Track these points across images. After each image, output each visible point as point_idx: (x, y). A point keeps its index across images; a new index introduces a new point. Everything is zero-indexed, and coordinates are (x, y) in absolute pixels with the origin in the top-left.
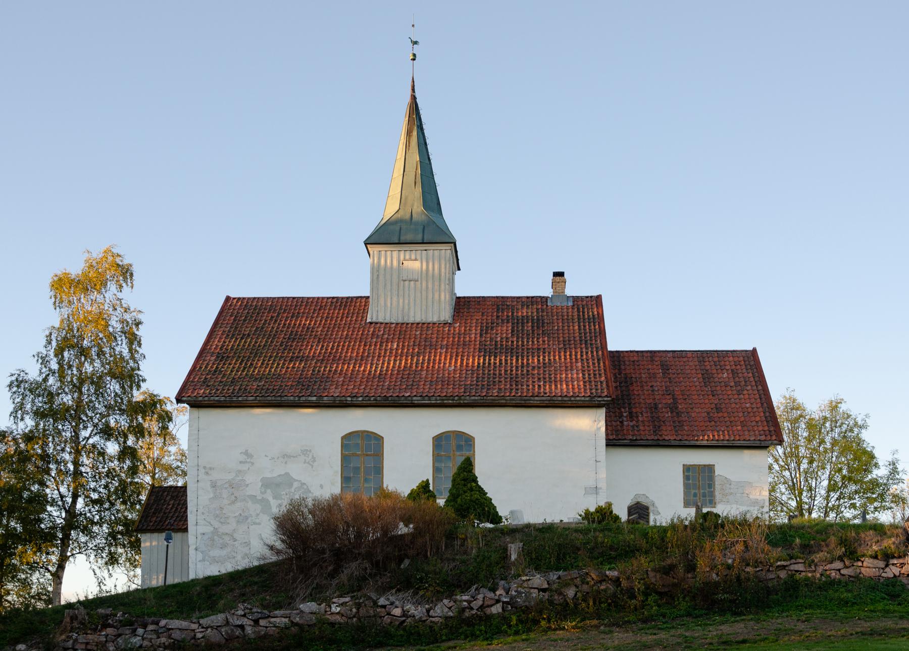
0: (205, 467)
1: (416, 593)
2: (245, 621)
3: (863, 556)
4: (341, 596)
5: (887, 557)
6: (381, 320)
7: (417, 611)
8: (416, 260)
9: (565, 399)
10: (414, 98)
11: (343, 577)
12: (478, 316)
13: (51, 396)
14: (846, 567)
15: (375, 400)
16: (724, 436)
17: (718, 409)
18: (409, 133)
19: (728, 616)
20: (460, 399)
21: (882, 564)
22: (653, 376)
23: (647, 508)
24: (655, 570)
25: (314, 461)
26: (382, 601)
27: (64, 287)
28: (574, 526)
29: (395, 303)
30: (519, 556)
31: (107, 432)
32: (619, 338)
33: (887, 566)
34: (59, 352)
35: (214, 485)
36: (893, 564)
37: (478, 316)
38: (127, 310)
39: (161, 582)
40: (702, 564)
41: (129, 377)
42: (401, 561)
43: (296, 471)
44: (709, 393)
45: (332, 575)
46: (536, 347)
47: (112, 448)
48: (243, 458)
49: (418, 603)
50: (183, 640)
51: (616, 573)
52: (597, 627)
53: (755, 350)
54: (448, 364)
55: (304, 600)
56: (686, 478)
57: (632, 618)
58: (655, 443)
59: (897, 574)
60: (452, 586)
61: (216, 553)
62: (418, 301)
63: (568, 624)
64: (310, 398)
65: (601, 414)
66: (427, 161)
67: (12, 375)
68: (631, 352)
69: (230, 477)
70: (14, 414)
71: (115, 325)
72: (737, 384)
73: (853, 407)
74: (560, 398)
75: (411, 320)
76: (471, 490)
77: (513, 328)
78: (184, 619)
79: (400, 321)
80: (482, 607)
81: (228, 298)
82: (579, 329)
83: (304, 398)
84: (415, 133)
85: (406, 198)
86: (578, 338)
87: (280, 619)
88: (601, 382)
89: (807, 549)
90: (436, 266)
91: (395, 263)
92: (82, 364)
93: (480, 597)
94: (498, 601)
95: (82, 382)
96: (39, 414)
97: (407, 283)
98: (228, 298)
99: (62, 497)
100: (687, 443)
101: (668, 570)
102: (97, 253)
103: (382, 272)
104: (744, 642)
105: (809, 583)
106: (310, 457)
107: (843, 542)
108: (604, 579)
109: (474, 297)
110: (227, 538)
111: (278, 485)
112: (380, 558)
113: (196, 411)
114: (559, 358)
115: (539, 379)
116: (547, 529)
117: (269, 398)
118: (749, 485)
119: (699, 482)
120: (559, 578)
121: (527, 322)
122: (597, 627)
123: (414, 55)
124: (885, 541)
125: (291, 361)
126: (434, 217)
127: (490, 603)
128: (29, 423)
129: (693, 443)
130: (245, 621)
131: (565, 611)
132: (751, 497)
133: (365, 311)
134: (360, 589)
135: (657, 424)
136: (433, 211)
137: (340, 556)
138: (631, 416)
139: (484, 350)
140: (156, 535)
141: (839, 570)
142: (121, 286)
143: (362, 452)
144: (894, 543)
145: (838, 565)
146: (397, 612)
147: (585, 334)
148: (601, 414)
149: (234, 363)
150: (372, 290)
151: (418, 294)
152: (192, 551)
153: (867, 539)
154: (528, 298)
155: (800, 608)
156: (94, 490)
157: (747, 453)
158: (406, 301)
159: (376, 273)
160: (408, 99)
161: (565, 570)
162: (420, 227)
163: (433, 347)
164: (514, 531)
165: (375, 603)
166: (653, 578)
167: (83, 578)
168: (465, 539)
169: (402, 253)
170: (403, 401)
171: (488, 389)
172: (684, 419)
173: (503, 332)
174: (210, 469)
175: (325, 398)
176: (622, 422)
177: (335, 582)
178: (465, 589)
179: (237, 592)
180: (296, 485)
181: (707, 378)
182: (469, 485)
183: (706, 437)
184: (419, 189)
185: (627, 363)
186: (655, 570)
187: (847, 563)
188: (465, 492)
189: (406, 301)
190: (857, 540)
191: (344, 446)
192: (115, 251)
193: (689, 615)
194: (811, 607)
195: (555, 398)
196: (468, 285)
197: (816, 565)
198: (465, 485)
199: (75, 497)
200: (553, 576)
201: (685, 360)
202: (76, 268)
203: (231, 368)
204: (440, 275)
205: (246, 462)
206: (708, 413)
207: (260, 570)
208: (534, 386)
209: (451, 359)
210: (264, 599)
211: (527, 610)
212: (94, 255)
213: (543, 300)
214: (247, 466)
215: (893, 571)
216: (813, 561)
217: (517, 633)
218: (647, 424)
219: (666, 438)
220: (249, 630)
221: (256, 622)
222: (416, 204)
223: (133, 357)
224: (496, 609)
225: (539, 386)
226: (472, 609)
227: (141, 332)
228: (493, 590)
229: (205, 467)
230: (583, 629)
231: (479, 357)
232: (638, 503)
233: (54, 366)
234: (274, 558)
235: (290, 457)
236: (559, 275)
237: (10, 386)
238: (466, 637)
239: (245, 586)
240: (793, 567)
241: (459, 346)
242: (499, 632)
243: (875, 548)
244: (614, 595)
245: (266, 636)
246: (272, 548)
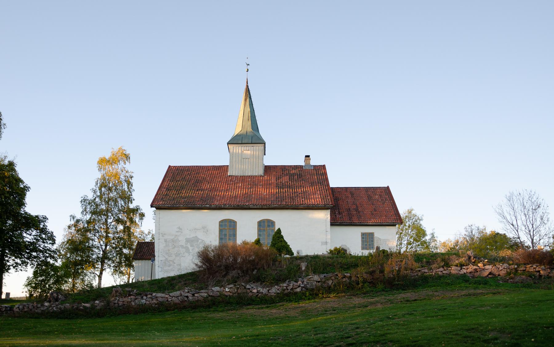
1: (261, 284)
2: (189, 294)
4: (229, 285)
5: (461, 265)
7: (265, 291)
11: (229, 277)
12: (274, 173)
13: (97, 205)
14: (445, 270)
16: (378, 221)
17: (375, 210)
18: (246, 100)
19: (400, 291)
21: (459, 268)
24: (366, 273)
26: (248, 287)
27: (103, 162)
31: (118, 221)
32: (334, 183)
34: (100, 189)
35: (166, 241)
37: (274, 173)
38: (127, 172)
39: (149, 279)
40: (387, 269)
41: (128, 198)
42: (253, 270)
43: (200, 235)
45: (224, 276)
46: (300, 185)
47: (121, 227)
48: (178, 230)
49: (263, 288)
50: (163, 302)
51: (349, 275)
52: (344, 296)
53: (388, 187)
54: (264, 192)
55: (212, 286)
56: (363, 238)
57: (359, 292)
60: (278, 280)
61: (166, 268)
63: (332, 295)
65: (329, 210)
69: (173, 237)
70: (82, 212)
71: (122, 177)
72: (382, 200)
73: (417, 212)
75: (247, 175)
76: (281, 241)
78: (163, 293)
80: (292, 289)
81: (170, 166)
84: (248, 100)
87: (204, 294)
89: (428, 263)
91: (240, 151)
92: (109, 194)
93: (291, 285)
94: (299, 286)
95: (109, 200)
96: (93, 213)
98: (170, 166)
99: (101, 245)
101: (372, 273)
102: (116, 149)
104: (415, 300)
105: (431, 277)
107: (443, 260)
108: (345, 277)
110: (171, 262)
112: (245, 269)
113: (158, 211)
114: (309, 189)
116: (316, 257)
118: (388, 239)
119: (367, 240)
120: (325, 276)
122: (344, 296)
126: (256, 133)
127: (296, 287)
128: (88, 217)
129: (366, 224)
130: (189, 294)
131: (329, 290)
133: (227, 171)
134: (236, 282)
135: (350, 216)
137: (228, 268)
138: (339, 213)
139: (278, 186)
140: (140, 261)
142: (125, 162)
143: (227, 228)
145: (441, 269)
146: (255, 291)
148: (329, 210)
149: (174, 192)
150: (230, 162)
152: (157, 267)
155: (430, 286)
156: (114, 243)
157: (387, 227)
160: (245, 87)
161: (327, 273)
162: (250, 137)
163: (257, 185)
164: (301, 258)
165: (245, 288)
166: (365, 276)
167: (109, 279)
168: (280, 262)
170: (245, 207)
173: (285, 179)
177: (225, 279)
178: (284, 281)
179: (183, 283)
180: (200, 241)
181: (369, 198)
184: (250, 122)
186: (366, 273)
187: (445, 268)
190: (449, 259)
191: (220, 225)
192: (123, 148)
193: (383, 291)
194: (434, 286)
196: (269, 161)
199: (106, 246)
200: (322, 276)
203: (172, 193)
207: (192, 274)
210: (195, 286)
211: (313, 290)
213: (301, 167)
214: (180, 233)
215: (464, 271)
217: (309, 299)
220: (190, 298)
221: (193, 295)
223: (129, 191)
224: (298, 290)
226: (288, 289)
227: (133, 181)
228: (296, 282)
230: (339, 297)
233: (99, 194)
234: (198, 269)
237: (81, 202)
238: (287, 301)
239: (186, 281)
240: (423, 271)
241: (267, 185)
242: (301, 299)
243: (457, 262)
244: (350, 283)
245: (198, 301)
246: (196, 265)
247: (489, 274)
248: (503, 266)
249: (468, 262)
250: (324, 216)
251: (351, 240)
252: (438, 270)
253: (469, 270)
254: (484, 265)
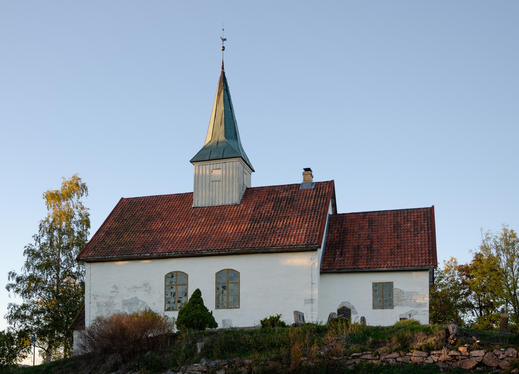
0: (94, 295)
3: (412, 349)
5: (429, 349)
6: (199, 206)
8: (219, 169)
9: (291, 247)
10: (223, 73)
15: (181, 253)
18: (219, 94)
20: (229, 251)
21: (425, 354)
22: (361, 228)
23: (350, 310)
25: (150, 290)
27: (53, 197)
28: (246, 330)
29: (207, 195)
30: (202, 350)
32: (344, 206)
33: (429, 355)
35: (98, 305)
36: (433, 354)
43: (141, 296)
44: (396, 236)
56: (374, 291)
58: (353, 270)
59: (436, 361)
62: (221, 194)
64: (146, 255)
66: (229, 110)
67: (26, 247)
68: (352, 213)
74: (288, 247)
75: (217, 204)
77: (274, 204)
79: (211, 205)
82: (314, 203)
83: (143, 255)
85: (216, 133)
86: (311, 209)
88: (316, 235)
89: (375, 345)
90: (231, 172)
91: (208, 172)
97: (214, 183)
100: (373, 269)
103: (200, 178)
106: (148, 287)
109: (257, 188)
111: (131, 304)
115: (279, 235)
117: (125, 256)
121: (284, 201)
123: (224, 47)
124: (429, 339)
125: (143, 233)
126: (232, 143)
132: (417, 301)
136: (232, 139)
138: (341, 254)
141: (396, 358)
144: (435, 340)
145: (395, 355)
147: (316, 205)
151: (221, 189)
153: (418, 337)
154: (288, 185)
157: (414, 274)
158: (214, 194)
159: (197, 178)
160: (219, 74)
162: (225, 147)
169: (201, 166)
171: (247, 244)
172: (375, 254)
174: (97, 296)
175: (154, 254)
176: (334, 258)
180: (140, 303)
182: (196, 306)
183: (386, 266)
184: (223, 127)
185: (348, 221)
188: (193, 310)
189: (214, 194)
195: (285, 247)
196: (258, 180)
197: (379, 356)
198: (193, 306)
201: (385, 216)
202: (57, 187)
204: (233, 177)
205: (115, 291)
206: (391, 250)
208: (274, 240)
209: (232, 226)
212: (67, 180)
213: (298, 186)
214: (115, 293)
216: (378, 352)
218: (350, 258)
219: (360, 267)
222: (221, 136)
225: (278, 240)
229: (94, 295)
231: (249, 224)
232: (344, 307)
235: (138, 288)
236: (308, 170)
240: (363, 357)
247: (477, 365)
248: (506, 353)
249: (440, 343)
250: (309, 262)
251: (355, 292)
252: (388, 356)
253: (442, 358)
254: (469, 350)
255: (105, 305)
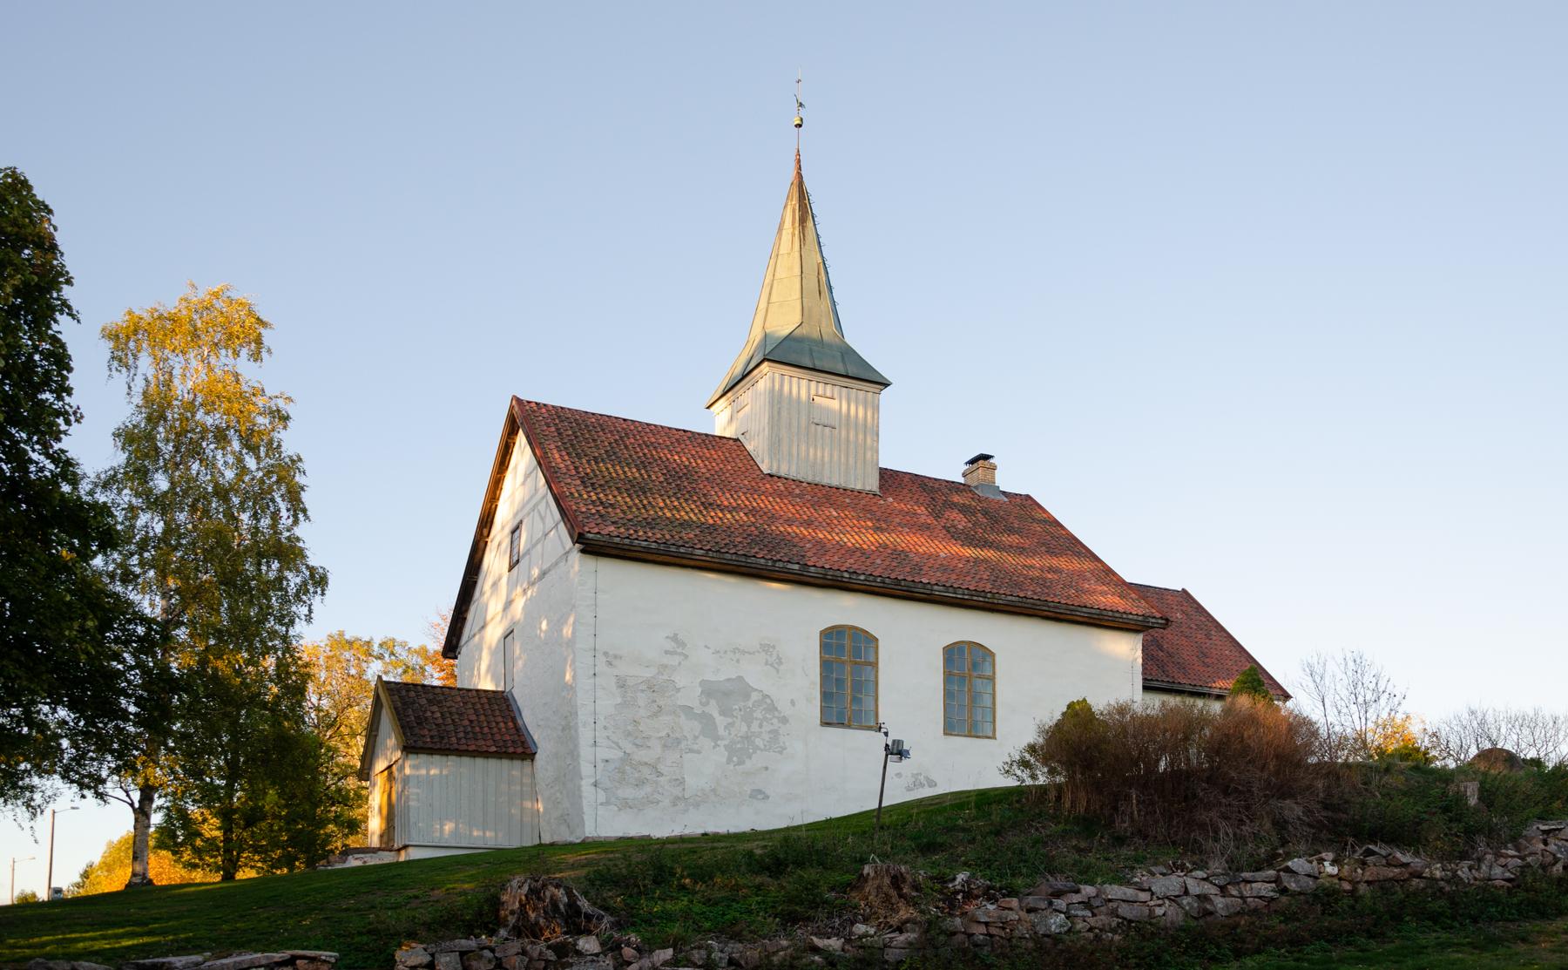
0: (606, 654)
25: (780, 663)
29: (803, 454)
35: (622, 684)
160: (791, 174)
174: (616, 657)
180: (755, 696)
229: (606, 654)
255: (643, 687)
